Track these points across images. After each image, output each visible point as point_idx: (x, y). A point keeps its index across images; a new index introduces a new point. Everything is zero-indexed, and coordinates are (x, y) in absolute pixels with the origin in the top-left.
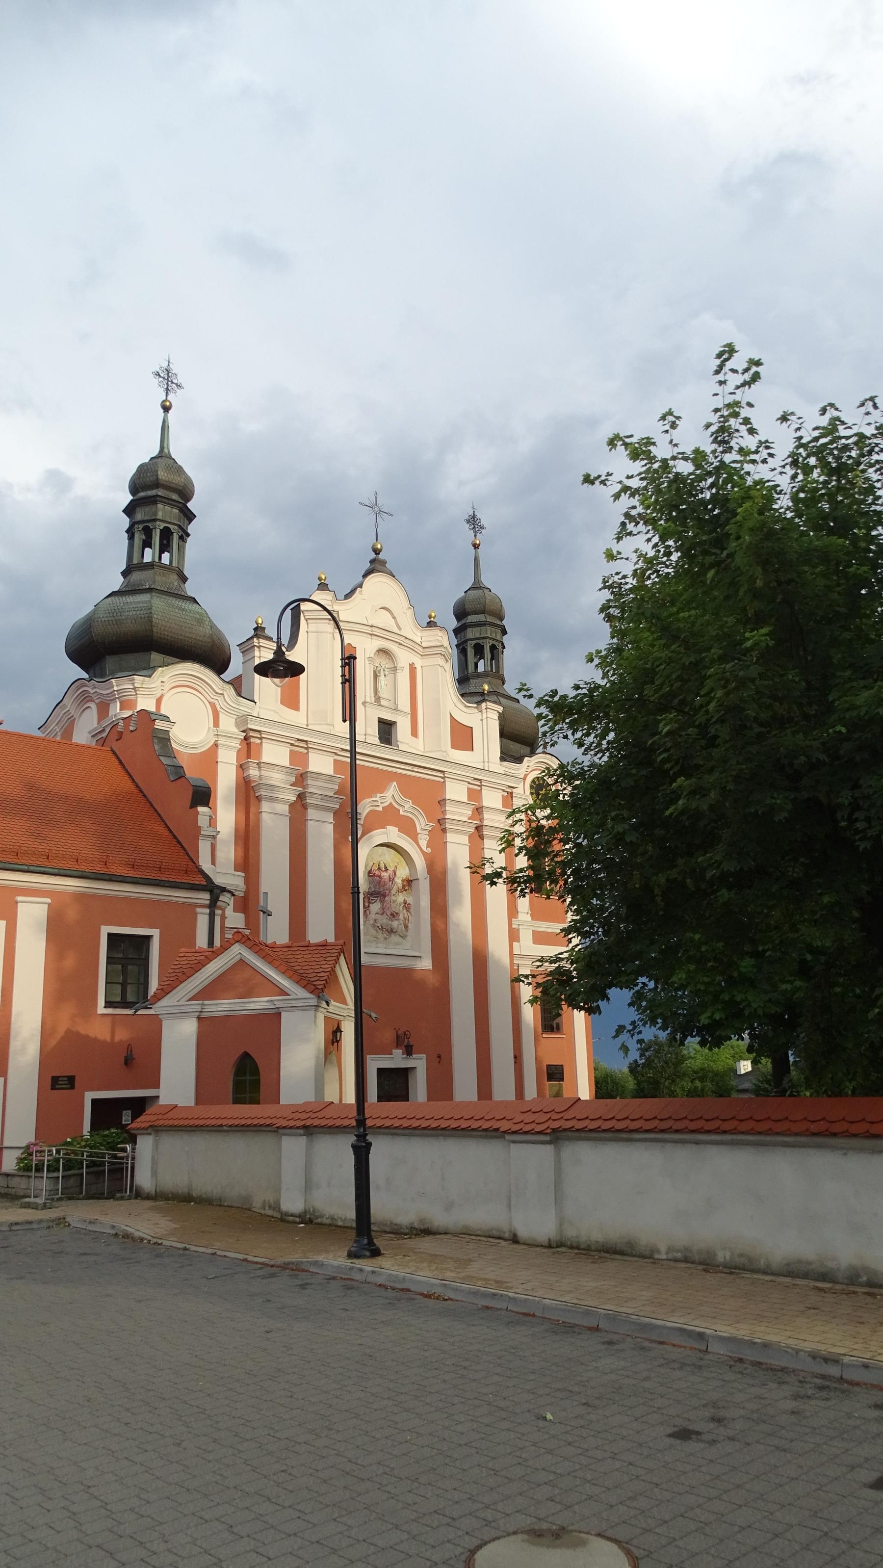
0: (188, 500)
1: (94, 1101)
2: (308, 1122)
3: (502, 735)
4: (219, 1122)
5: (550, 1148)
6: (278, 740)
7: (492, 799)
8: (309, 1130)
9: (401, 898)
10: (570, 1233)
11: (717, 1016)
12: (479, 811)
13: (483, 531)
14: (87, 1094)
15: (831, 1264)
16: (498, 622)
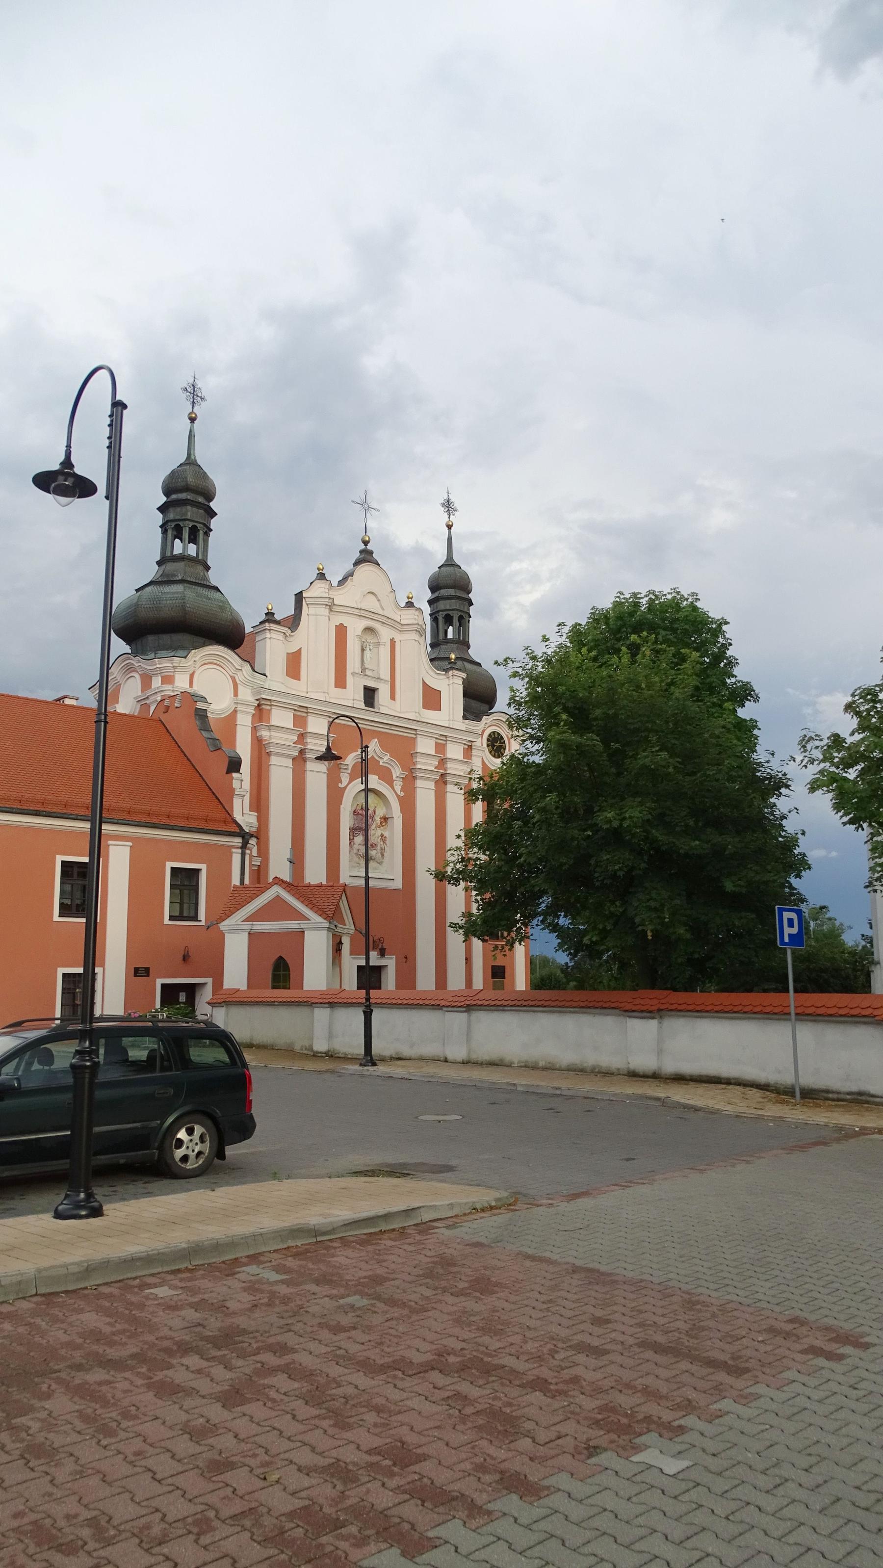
0: (211, 500)
1: (163, 986)
2: (331, 1000)
3: (465, 695)
4: (272, 1000)
5: (465, 1014)
6: (285, 707)
7: (454, 751)
8: (332, 1005)
9: (379, 832)
10: (474, 1057)
11: (594, 939)
12: (443, 762)
13: (456, 513)
14: (211, 979)
15: (585, 1065)
16: (465, 596)
